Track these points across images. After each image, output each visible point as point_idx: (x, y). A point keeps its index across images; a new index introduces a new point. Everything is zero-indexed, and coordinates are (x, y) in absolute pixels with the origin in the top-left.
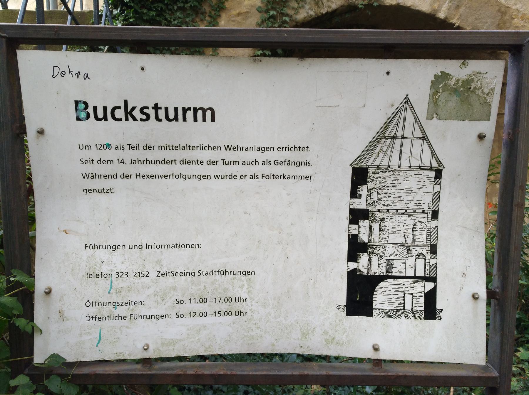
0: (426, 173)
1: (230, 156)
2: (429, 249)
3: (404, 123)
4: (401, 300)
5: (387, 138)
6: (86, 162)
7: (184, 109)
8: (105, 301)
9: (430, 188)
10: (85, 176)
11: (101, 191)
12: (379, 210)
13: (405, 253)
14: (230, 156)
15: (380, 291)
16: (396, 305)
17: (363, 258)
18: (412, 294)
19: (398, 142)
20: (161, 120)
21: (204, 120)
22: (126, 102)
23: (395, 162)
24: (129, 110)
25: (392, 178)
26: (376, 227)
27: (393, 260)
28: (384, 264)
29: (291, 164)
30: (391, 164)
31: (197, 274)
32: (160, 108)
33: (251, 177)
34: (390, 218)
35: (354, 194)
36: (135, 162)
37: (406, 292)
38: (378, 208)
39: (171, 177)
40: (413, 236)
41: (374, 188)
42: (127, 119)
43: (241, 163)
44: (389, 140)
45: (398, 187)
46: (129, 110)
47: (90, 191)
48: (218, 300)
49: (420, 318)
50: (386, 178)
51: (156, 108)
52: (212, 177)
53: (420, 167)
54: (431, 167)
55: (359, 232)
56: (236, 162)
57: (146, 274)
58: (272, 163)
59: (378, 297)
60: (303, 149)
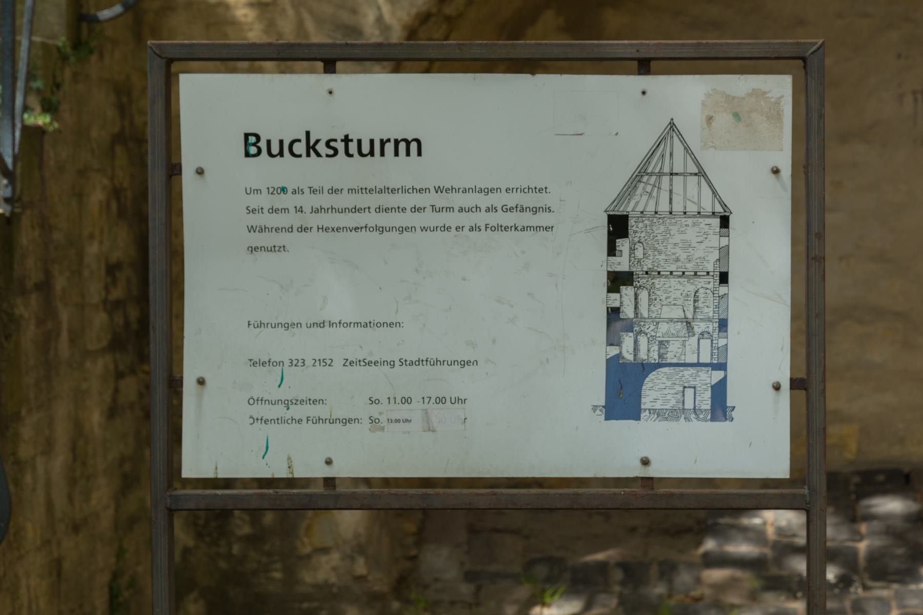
0: (708, 221)
1: (441, 200)
2: (717, 325)
3: (671, 155)
4: (679, 396)
5: (651, 174)
6: (253, 211)
7: (382, 141)
8: (274, 398)
9: (715, 240)
10: (251, 229)
11: (273, 249)
12: (647, 273)
13: (685, 331)
14: (441, 200)
15: (650, 385)
16: (673, 402)
17: (628, 341)
18: (694, 388)
19: (666, 180)
20: (352, 156)
21: (408, 154)
22: (308, 133)
23: (664, 207)
24: (312, 144)
25: (662, 228)
26: (644, 296)
27: (668, 342)
28: (656, 348)
29: (524, 212)
30: (660, 209)
31: (397, 363)
32: (352, 140)
33: (471, 229)
34: (662, 283)
35: (612, 250)
36: (317, 211)
37: (686, 385)
38: (645, 269)
39: (364, 230)
40: (695, 308)
41: (639, 242)
42: (308, 155)
43: (456, 209)
44: (654, 178)
45: (671, 241)
46: (312, 144)
47: (256, 249)
48: (427, 400)
49: (705, 420)
50: (654, 228)
51: (347, 140)
52: (418, 229)
53: (699, 213)
54: (713, 213)
55: (621, 303)
56: (450, 209)
57: (329, 362)
58: (499, 209)
59: (648, 392)
60: (540, 190)
